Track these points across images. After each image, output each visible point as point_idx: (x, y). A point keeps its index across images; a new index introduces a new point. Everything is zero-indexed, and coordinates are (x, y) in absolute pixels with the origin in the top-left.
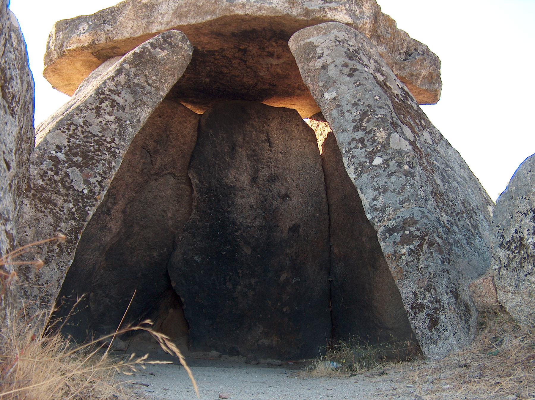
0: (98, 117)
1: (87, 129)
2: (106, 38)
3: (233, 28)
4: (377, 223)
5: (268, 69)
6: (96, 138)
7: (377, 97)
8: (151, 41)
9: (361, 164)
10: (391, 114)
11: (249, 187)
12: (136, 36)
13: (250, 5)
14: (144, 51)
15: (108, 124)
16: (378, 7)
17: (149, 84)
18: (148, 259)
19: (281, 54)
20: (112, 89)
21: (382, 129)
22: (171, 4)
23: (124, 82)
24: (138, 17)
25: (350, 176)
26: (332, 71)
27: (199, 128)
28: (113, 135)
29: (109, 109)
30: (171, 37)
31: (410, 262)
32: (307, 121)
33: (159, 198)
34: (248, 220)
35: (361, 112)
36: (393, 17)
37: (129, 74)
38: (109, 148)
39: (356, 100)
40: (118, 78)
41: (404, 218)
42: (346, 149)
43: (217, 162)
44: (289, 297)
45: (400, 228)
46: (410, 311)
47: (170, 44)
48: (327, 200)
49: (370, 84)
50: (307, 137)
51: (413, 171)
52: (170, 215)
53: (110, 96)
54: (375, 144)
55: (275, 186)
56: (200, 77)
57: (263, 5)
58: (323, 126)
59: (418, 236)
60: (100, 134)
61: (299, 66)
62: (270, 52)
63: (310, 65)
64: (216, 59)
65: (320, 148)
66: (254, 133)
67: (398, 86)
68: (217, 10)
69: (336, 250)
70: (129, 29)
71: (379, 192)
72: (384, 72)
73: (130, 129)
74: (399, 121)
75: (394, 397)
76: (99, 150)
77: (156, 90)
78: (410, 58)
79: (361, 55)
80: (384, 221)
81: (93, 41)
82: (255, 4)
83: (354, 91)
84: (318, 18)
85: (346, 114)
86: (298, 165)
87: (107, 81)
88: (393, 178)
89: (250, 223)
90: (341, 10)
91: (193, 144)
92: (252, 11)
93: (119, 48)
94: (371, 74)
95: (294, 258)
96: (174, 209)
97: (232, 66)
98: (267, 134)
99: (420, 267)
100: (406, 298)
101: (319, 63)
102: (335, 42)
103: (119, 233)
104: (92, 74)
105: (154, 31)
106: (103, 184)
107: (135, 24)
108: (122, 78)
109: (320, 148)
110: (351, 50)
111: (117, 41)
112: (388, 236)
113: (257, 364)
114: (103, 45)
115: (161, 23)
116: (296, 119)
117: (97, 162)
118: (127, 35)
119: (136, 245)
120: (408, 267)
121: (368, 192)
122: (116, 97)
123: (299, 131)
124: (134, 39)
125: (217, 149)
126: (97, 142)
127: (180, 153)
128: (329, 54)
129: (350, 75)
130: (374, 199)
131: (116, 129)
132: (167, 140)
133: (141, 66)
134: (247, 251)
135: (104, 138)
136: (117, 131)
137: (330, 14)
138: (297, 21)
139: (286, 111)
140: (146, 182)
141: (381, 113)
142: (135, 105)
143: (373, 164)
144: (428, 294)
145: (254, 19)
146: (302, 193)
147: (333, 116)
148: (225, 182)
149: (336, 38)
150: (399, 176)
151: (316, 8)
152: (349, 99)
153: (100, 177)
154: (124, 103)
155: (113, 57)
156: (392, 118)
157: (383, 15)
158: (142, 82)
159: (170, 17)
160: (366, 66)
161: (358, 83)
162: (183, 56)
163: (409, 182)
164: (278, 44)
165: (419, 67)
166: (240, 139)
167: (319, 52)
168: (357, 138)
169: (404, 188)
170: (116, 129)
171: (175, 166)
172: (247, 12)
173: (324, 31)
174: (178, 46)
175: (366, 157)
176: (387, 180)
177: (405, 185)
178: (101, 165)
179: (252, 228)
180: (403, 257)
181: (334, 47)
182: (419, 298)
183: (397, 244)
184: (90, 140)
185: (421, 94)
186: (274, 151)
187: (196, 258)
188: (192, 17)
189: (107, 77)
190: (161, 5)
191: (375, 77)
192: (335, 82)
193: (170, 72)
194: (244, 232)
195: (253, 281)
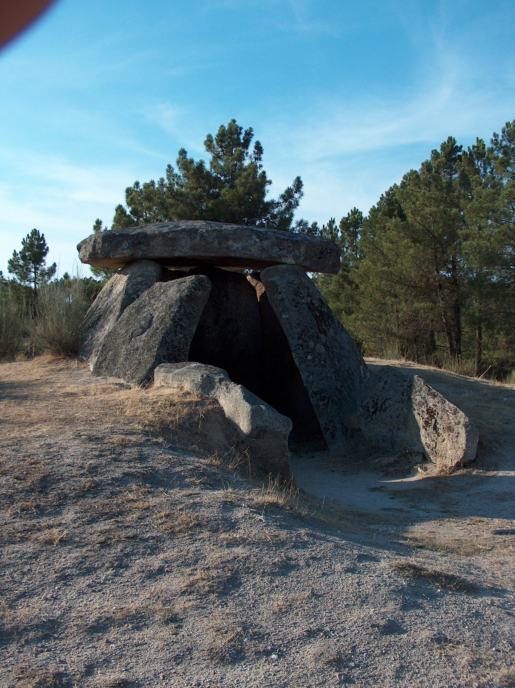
9: (302, 358)
17: (194, 311)
26: (286, 303)
29: (180, 330)
65: (258, 298)
81: (133, 254)
85: (294, 328)
88: (317, 368)
101: (279, 297)
109: (258, 298)
129: (296, 306)
130: (308, 377)
144: (331, 424)
167: (280, 290)
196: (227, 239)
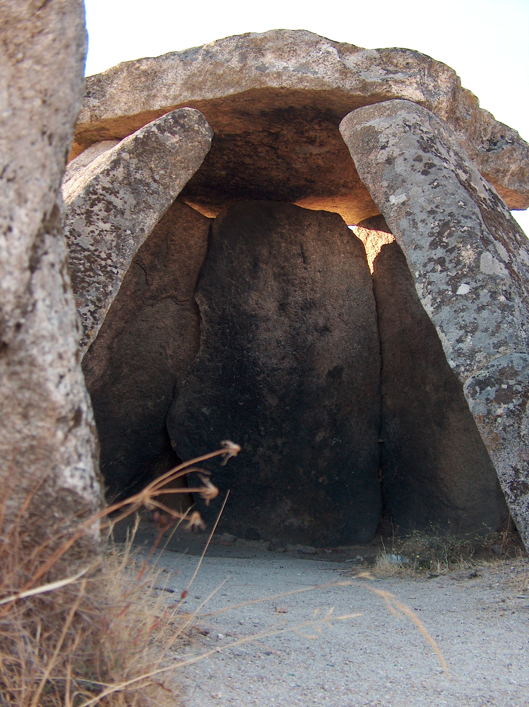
0: (88, 224)
1: (74, 240)
2: (92, 116)
3: (264, 105)
4: (463, 372)
5: (306, 160)
6: (87, 253)
7: (461, 203)
8: (158, 122)
9: (441, 293)
10: (481, 226)
11: (275, 317)
12: (132, 114)
13: (287, 75)
14: (148, 135)
15: (102, 233)
16: (457, 80)
17: (155, 181)
18: (140, 410)
19: (325, 140)
20: (107, 186)
21: (469, 247)
22: (180, 72)
23: (122, 178)
24: (135, 88)
25: (426, 308)
26: (400, 167)
27: (210, 237)
28: (109, 249)
29: (103, 214)
30: (185, 117)
31: (509, 426)
32: (354, 229)
33: (156, 330)
34: (274, 361)
35: (440, 223)
36: (475, 92)
37: (129, 167)
38: (104, 266)
39: (433, 206)
40: (115, 172)
41: (500, 367)
42: (420, 272)
43: (234, 282)
44: (326, 463)
45: (495, 380)
46: (509, 492)
47: (183, 126)
48: (379, 335)
49: (451, 185)
50: (354, 250)
51: (511, 304)
52: (169, 352)
53: (105, 196)
54: (460, 266)
55: (311, 316)
56: (214, 169)
57: (305, 75)
58: (375, 236)
59: (520, 392)
60: (92, 248)
61: (355, 158)
62: (311, 138)
63: (370, 157)
64: (238, 146)
65: (371, 265)
66: (283, 244)
67: (484, 186)
68: (244, 81)
69: (389, 402)
70: (123, 104)
71: (466, 332)
72: (467, 168)
73: (131, 241)
74: (491, 236)
75: (506, 613)
76: (91, 269)
77: (164, 188)
78: (496, 147)
79: (438, 146)
80: (473, 370)
82: (295, 73)
83: (430, 194)
84: (380, 94)
85: (420, 225)
86: (342, 287)
87: (101, 176)
88: (485, 313)
89: (277, 364)
90: (411, 83)
91: (202, 259)
92: (290, 82)
93: (108, 130)
94: (452, 171)
95: (335, 411)
96: (176, 343)
97: (257, 156)
98: (301, 246)
99: (522, 434)
100: (503, 475)
101: (382, 156)
102: (404, 127)
103: (102, 376)
104: (72, 164)
105: (157, 107)
106: (97, 315)
107: (131, 97)
108: (120, 173)
109: (371, 265)
110: (425, 139)
111: (105, 121)
112: (478, 391)
113: (284, 551)
114: (86, 126)
115: (166, 98)
116: (340, 227)
117: (89, 286)
118: (120, 113)
119: (125, 391)
120: (506, 433)
121: (450, 331)
122: (112, 198)
123: (343, 242)
124: (128, 118)
125: (234, 265)
126: (87, 258)
127: (185, 269)
128: (396, 143)
129: (425, 173)
131: (113, 241)
132: (167, 253)
133: (145, 156)
134: (272, 401)
135: (96, 253)
136: (114, 244)
137: (396, 88)
138: (350, 97)
139: (326, 216)
140: (140, 308)
141: (467, 225)
142: (137, 209)
143: (457, 293)
145: (292, 94)
146: (346, 325)
147: (402, 228)
148: (245, 309)
149: (405, 121)
150: (493, 310)
151: (377, 81)
152: (424, 204)
153: (93, 306)
154: (123, 205)
155: (98, 141)
156: (482, 232)
157: (463, 90)
158: (146, 178)
159: (179, 89)
160: (445, 160)
161: (435, 184)
162: (200, 142)
163: (507, 318)
164: (322, 128)
165: (507, 160)
166: (265, 252)
167: (382, 139)
168: (435, 257)
169: (500, 327)
170: (113, 241)
171: (178, 287)
172: (284, 85)
173: (389, 112)
174: (193, 130)
175: (447, 284)
176: (476, 316)
177: (501, 322)
178: (94, 289)
179: (280, 371)
180: (499, 420)
181: (402, 134)
182: (521, 476)
183: (491, 401)
184: (79, 256)
185: (508, 196)
186: (309, 269)
187: (204, 410)
188: (208, 89)
189: (99, 171)
190: (166, 73)
191: (457, 175)
192: (405, 182)
193: (183, 165)
194: (268, 375)
195: (279, 442)
196: (260, 51)
